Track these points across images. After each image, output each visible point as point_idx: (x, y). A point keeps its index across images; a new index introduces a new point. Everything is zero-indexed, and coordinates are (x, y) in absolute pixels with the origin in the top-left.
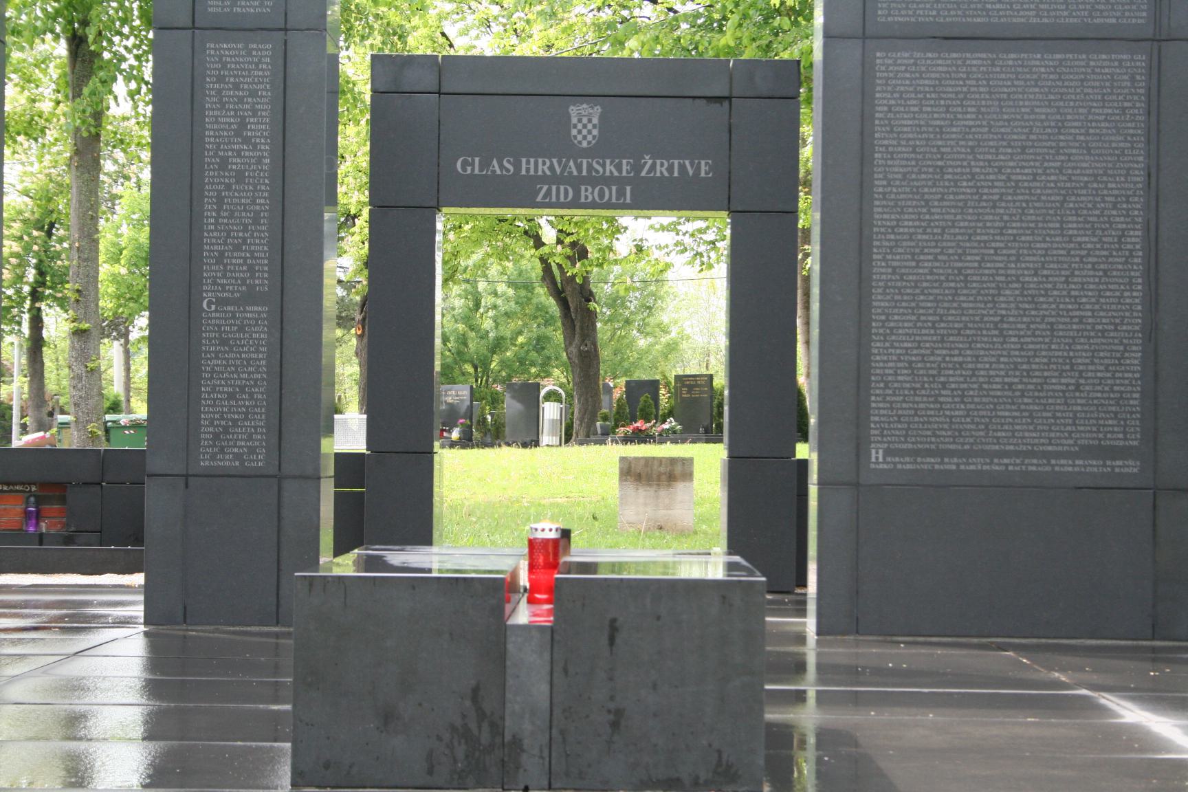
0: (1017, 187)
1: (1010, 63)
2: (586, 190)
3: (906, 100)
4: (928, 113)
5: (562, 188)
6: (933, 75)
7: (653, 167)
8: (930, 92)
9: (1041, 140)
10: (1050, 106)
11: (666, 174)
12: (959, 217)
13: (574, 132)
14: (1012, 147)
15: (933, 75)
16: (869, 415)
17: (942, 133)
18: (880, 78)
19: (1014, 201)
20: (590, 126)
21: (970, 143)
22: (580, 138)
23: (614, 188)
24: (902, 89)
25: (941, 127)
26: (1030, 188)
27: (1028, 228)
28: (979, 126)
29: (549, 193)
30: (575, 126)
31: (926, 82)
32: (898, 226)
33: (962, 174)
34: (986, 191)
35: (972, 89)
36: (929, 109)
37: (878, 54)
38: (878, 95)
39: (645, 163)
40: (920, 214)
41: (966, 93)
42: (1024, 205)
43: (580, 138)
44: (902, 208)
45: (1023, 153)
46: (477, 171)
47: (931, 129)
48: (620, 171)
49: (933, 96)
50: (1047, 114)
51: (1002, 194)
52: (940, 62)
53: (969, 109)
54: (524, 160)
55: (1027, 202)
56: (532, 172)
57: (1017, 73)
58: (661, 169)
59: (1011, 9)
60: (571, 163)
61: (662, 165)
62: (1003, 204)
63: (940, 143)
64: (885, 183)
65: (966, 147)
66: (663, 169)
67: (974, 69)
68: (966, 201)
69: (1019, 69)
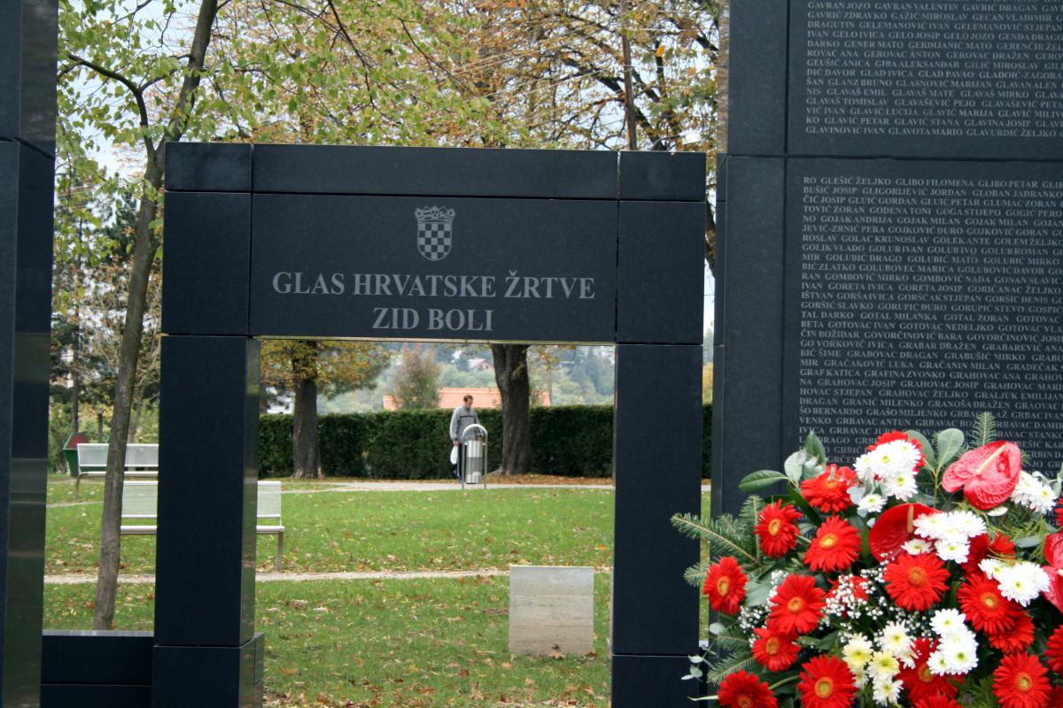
0: (1003, 370)
1: (994, 193)
2: (436, 314)
3: (845, 245)
4: (877, 264)
5: (405, 311)
6: (884, 210)
7: (520, 287)
8: (880, 235)
9: (1037, 304)
10: (1050, 256)
11: (537, 295)
12: (921, 413)
13: (421, 241)
14: (997, 314)
15: (884, 210)
16: (799, 367)
17: (896, 292)
18: (808, 214)
19: (1000, 391)
20: (441, 234)
21: (937, 308)
22: (428, 248)
23: (471, 312)
24: (840, 229)
25: (895, 284)
26: (1022, 373)
27: (1020, 430)
28: (948, 283)
29: (388, 318)
30: (422, 234)
31: (875, 220)
32: (834, 425)
33: (926, 351)
34: (959, 375)
35: (940, 231)
36: (878, 258)
37: (806, 180)
38: (805, 238)
39: (511, 281)
40: (865, 407)
41: (932, 236)
42: (1014, 396)
43: (428, 248)
44: (840, 398)
45: (1012, 322)
46: (298, 290)
47: (881, 287)
48: (479, 291)
49: (884, 239)
50: (1046, 267)
51: (982, 381)
52: (894, 191)
53: (936, 259)
54: (358, 277)
55: (1018, 392)
56: (368, 292)
57: (1003, 209)
58: (531, 290)
59: (996, 117)
60: (418, 281)
61: (532, 284)
62: (984, 395)
63: (894, 307)
64: (815, 363)
65: (931, 313)
66: (533, 289)
67: (942, 202)
68: (931, 390)
69: (1007, 203)
